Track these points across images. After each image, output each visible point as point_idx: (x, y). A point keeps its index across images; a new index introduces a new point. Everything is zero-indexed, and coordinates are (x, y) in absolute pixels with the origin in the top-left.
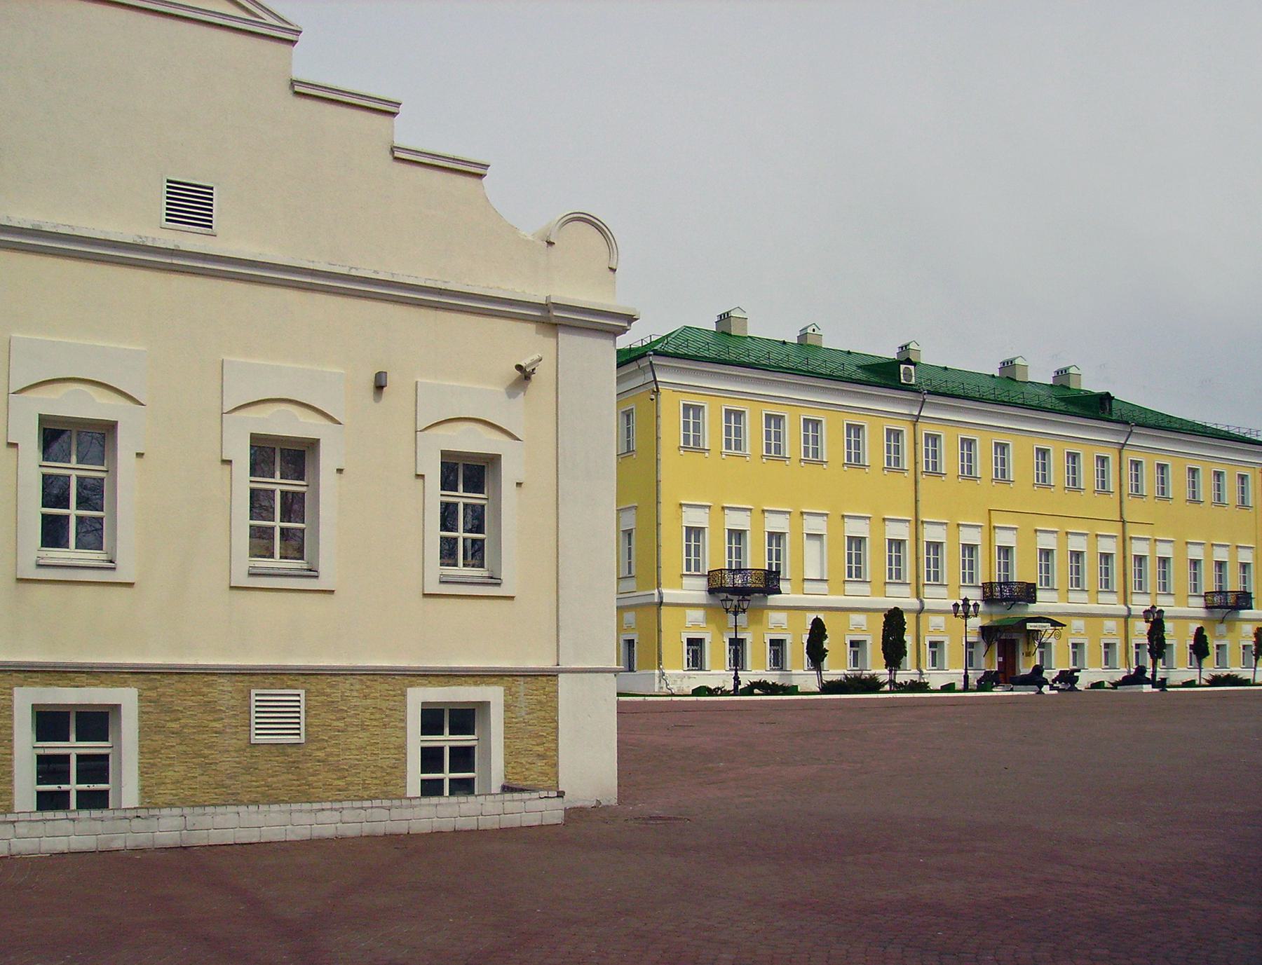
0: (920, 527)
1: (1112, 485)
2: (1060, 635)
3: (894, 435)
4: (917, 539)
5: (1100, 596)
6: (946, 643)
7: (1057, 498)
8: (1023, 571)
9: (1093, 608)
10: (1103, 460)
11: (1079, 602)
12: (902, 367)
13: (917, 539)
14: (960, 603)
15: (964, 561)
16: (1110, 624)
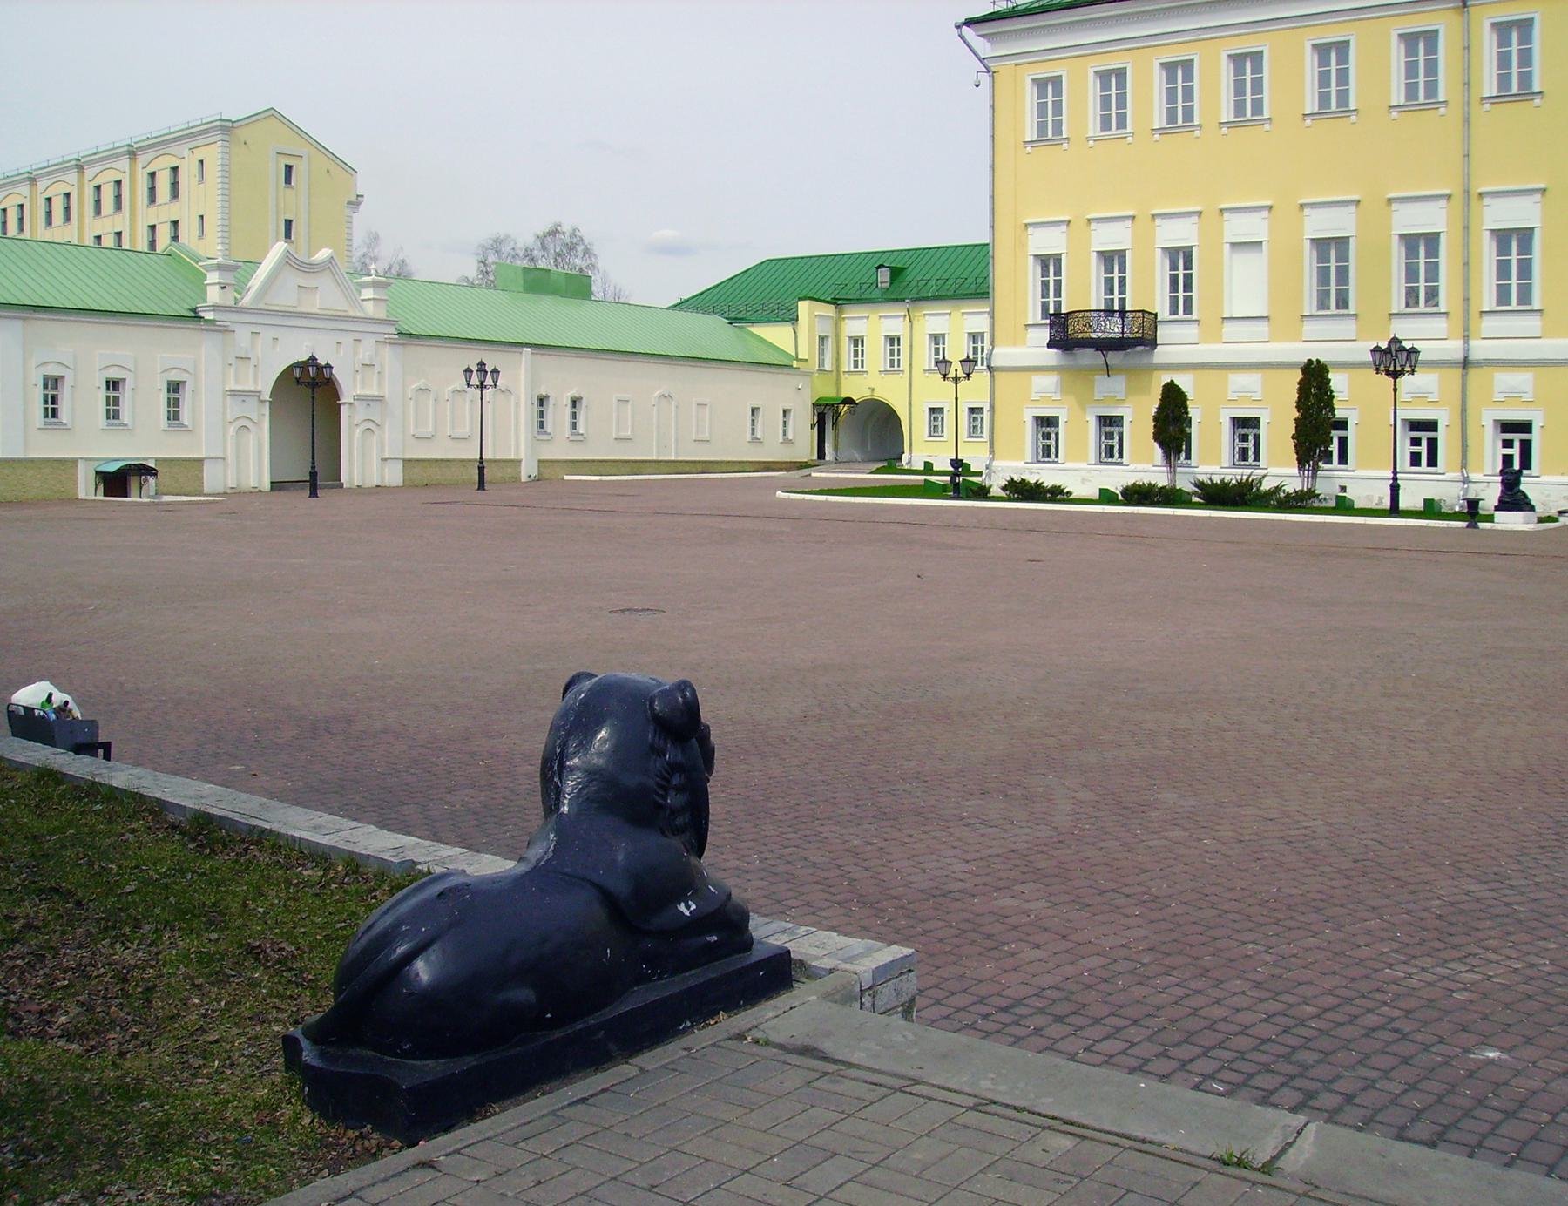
0: (1474, 202)
14: (475, 368)
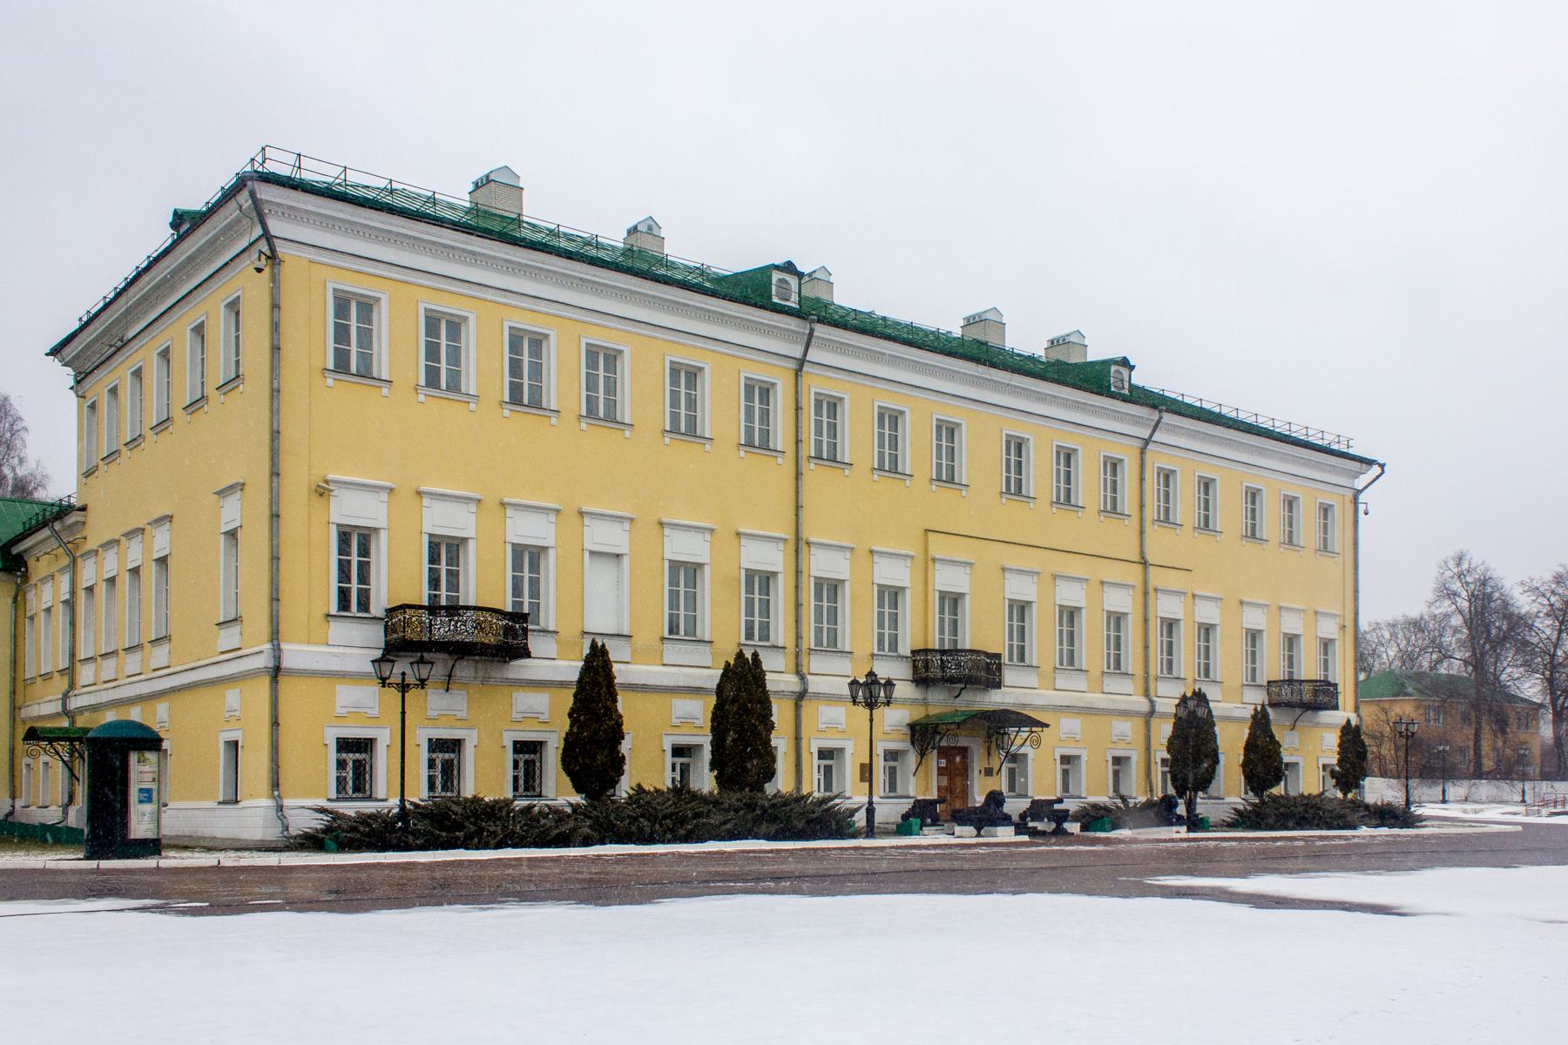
1: (1128, 503)
2: (1039, 742)
3: (759, 392)
4: (798, 572)
5: (1107, 680)
6: (1084, 759)
7: (1037, 517)
8: (982, 632)
9: (1096, 699)
10: (1326, 510)
11: (1075, 689)
12: (1113, 368)
13: (798, 572)
15: (1011, 627)
16: (1123, 727)
